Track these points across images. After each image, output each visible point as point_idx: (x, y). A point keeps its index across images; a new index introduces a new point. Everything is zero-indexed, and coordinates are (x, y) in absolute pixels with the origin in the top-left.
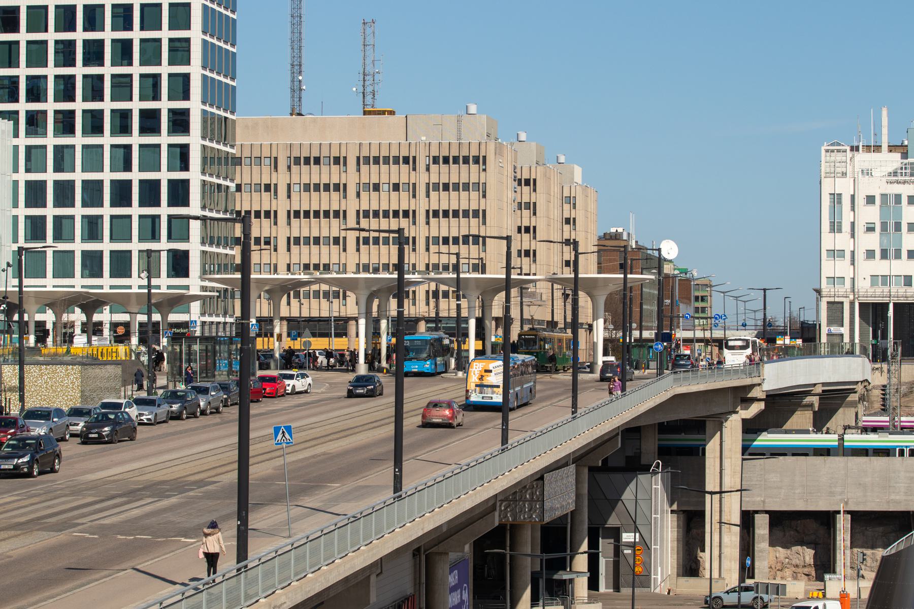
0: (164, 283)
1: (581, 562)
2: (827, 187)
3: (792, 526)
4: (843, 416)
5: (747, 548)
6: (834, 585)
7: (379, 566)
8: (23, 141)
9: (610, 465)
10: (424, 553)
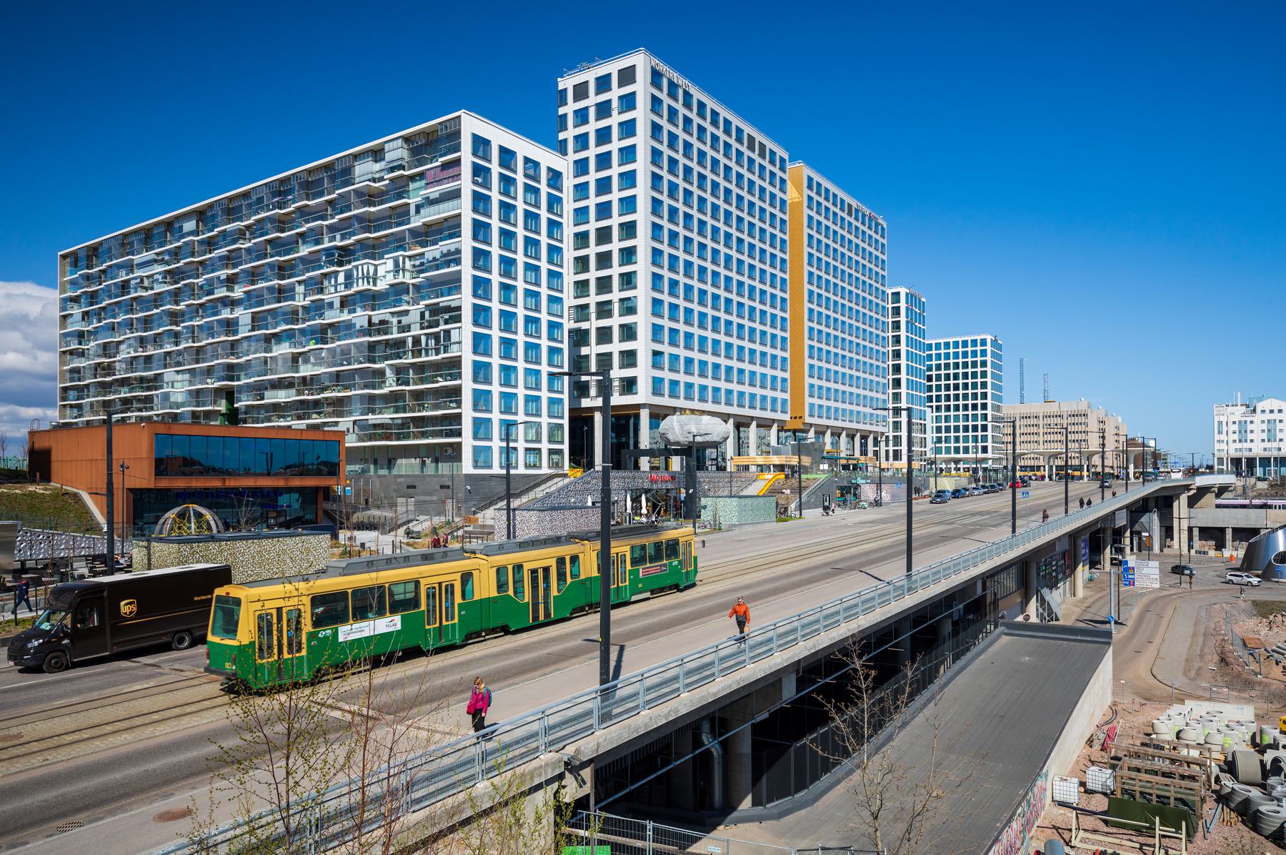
0: (980, 455)
1: (1128, 541)
2: (1217, 419)
3: (1206, 533)
4: (1226, 495)
5: (1190, 539)
6: (1227, 553)
7: (1059, 539)
8: (935, 414)
9: (1138, 509)
10: (1073, 536)
